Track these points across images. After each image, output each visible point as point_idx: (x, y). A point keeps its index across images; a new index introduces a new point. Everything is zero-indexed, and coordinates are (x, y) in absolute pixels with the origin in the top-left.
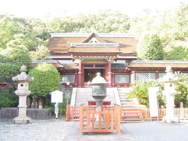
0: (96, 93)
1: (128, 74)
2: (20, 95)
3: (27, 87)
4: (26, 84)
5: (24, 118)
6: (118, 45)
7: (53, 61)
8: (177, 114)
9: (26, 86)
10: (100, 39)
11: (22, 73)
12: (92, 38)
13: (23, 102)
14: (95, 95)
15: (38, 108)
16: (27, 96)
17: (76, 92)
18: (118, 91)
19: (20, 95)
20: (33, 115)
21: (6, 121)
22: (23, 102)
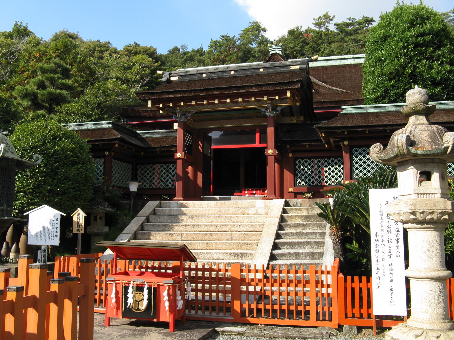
7: (102, 124)
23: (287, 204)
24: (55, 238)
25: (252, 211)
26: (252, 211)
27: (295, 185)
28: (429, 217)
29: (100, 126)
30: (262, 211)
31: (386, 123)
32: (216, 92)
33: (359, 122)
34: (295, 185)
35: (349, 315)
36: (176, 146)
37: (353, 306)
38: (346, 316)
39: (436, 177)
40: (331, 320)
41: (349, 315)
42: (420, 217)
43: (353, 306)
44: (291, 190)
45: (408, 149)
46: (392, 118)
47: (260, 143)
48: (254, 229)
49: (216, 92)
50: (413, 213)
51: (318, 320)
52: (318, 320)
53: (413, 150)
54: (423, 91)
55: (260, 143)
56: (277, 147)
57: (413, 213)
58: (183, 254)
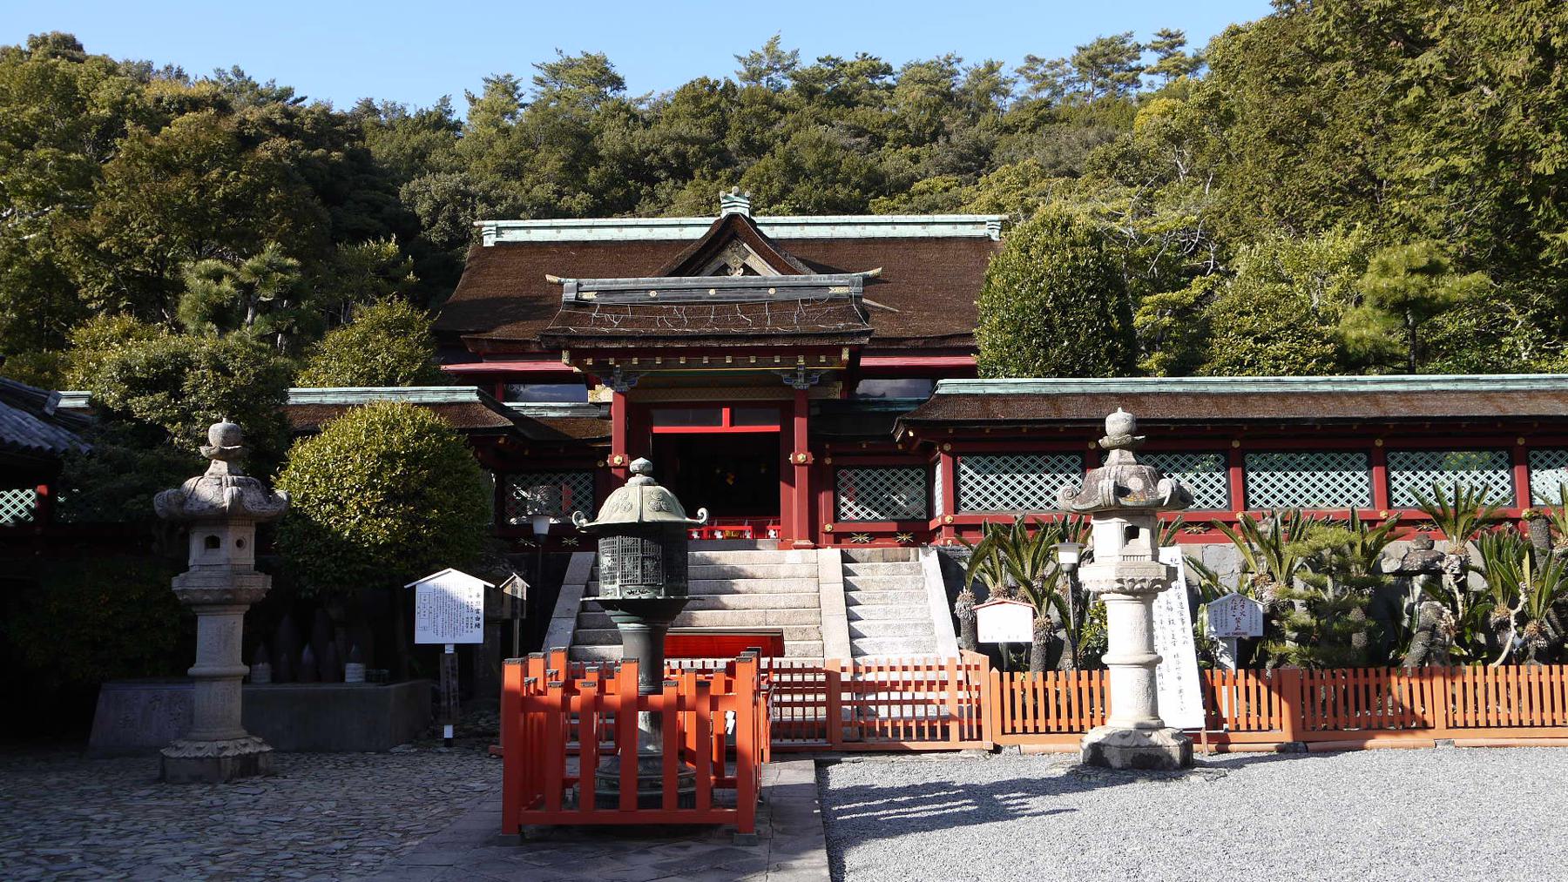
0: (616, 586)
1: (1075, 453)
2: (197, 605)
3: (248, 557)
4: (240, 536)
5: (224, 744)
6: (852, 283)
7: (455, 392)
8: (1087, 713)
9: (238, 551)
10: (776, 252)
11: (1114, 455)
12: (723, 248)
13: (220, 642)
14: (609, 597)
15: (342, 678)
16: (248, 608)
17: (587, 576)
18: (846, 572)
19: (197, 605)
20: (300, 731)
21: (1160, 779)
22: (220, 642)
23: (846, 559)
24: (476, 630)
25: (783, 571)
26: (783, 571)
27: (836, 519)
28: (1138, 586)
29: (450, 398)
30: (804, 570)
31: (1022, 416)
32: (708, 344)
33: (971, 413)
34: (836, 519)
35: (1008, 729)
36: (609, 439)
37: (1013, 717)
38: (1003, 733)
39: (1144, 533)
40: (980, 738)
41: (1008, 729)
42: (1127, 586)
43: (1013, 717)
44: (828, 528)
45: (1117, 501)
46: (1029, 405)
47: (732, 424)
48: (800, 603)
49: (708, 344)
50: (1120, 581)
51: (962, 739)
52: (962, 739)
53: (1122, 501)
54: (1128, 416)
55: (732, 424)
56: (812, 447)
57: (1120, 581)
58: (772, 644)
